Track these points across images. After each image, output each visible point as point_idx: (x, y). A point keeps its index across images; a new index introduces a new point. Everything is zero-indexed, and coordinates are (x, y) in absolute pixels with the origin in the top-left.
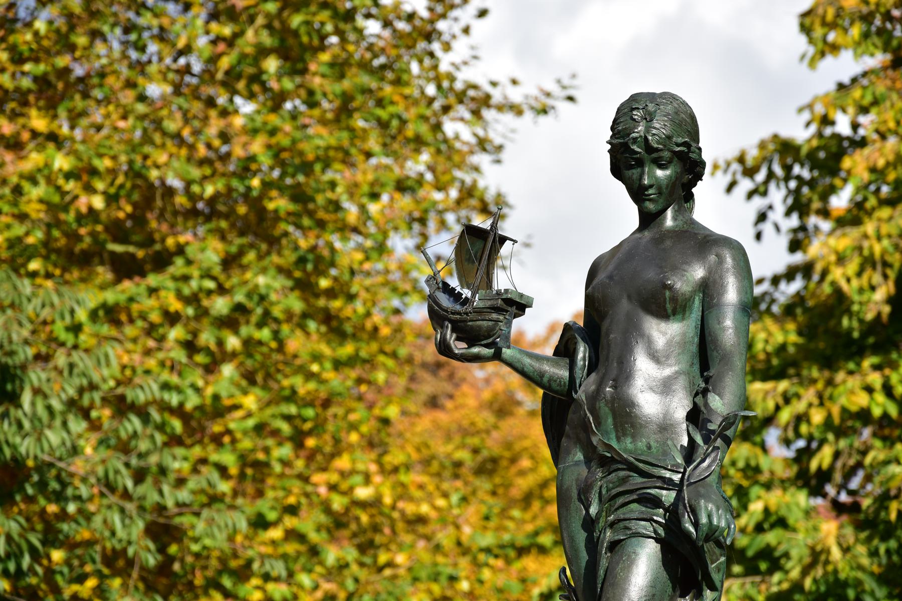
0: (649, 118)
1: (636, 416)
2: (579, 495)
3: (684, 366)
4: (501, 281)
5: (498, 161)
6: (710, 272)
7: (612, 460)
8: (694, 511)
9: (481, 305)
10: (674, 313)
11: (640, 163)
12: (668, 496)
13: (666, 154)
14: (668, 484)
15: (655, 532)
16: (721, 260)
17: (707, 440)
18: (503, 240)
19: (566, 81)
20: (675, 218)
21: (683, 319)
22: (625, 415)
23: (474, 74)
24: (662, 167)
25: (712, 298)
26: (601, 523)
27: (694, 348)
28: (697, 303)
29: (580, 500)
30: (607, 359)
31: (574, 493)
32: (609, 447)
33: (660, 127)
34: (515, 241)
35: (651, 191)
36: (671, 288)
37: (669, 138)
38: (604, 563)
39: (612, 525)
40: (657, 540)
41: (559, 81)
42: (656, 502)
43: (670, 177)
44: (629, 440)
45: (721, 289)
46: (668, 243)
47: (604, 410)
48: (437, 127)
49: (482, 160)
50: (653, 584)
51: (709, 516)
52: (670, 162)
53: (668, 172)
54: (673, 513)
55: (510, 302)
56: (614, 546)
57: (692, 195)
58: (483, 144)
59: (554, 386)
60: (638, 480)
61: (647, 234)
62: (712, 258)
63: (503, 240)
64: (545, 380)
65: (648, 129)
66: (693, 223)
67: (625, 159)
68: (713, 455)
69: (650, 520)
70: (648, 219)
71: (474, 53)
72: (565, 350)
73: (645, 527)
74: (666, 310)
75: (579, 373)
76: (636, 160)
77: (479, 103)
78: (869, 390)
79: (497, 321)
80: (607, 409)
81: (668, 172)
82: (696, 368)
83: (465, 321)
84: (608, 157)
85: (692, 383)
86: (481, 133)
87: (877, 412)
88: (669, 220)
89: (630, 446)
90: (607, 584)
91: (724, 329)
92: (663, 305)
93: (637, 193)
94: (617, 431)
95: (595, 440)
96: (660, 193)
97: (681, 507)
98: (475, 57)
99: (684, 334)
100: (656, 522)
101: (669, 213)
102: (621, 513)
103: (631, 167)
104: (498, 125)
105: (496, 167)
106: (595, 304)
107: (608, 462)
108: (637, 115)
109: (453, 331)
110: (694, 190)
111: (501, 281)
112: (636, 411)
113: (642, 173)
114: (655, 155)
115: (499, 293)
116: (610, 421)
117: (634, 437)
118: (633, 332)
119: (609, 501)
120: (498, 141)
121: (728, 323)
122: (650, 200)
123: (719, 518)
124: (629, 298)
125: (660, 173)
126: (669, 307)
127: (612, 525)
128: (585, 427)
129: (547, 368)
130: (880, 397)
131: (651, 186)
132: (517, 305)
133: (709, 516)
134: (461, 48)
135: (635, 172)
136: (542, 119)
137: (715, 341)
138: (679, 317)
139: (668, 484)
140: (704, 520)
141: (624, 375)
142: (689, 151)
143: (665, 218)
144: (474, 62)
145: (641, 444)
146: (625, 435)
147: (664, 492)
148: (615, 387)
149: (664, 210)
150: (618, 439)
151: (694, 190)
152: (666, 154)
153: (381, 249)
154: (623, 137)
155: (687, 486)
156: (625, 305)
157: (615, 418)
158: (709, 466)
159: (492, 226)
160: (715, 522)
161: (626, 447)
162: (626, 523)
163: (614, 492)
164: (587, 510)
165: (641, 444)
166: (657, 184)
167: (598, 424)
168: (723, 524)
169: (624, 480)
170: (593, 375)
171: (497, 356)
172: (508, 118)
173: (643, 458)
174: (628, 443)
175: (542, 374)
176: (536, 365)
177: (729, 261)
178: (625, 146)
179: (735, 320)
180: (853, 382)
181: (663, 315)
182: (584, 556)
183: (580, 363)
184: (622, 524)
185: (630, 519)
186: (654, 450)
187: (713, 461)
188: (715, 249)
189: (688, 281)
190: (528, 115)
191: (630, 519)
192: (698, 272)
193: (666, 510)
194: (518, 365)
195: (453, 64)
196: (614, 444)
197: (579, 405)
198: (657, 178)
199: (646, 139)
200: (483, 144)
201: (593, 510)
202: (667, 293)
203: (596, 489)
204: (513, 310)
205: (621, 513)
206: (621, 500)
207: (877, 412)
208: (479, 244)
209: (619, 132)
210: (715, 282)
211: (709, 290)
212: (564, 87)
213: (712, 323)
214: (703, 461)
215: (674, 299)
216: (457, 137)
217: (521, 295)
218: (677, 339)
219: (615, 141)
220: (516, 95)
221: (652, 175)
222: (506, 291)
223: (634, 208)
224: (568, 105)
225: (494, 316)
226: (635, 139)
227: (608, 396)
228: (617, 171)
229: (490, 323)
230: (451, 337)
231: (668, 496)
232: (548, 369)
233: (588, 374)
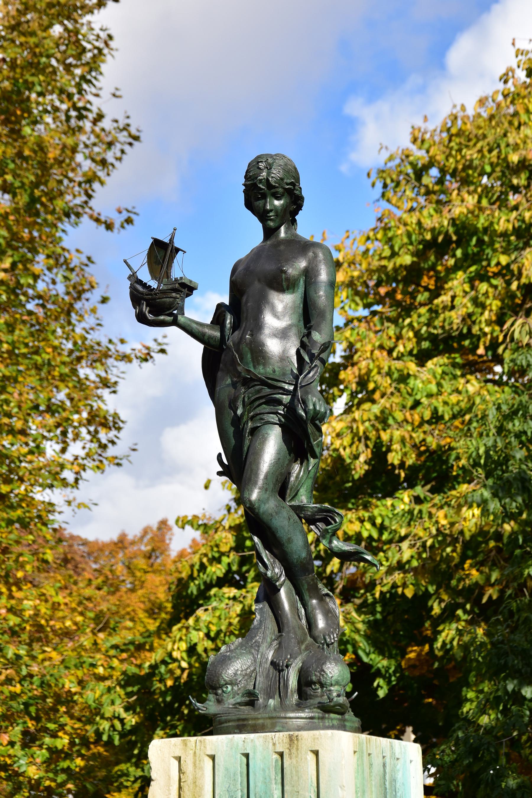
0: (269, 168)
1: (266, 352)
2: (230, 404)
3: (295, 321)
4: (176, 273)
5: (114, 392)
6: (309, 263)
7: (252, 380)
8: (304, 402)
9: (165, 288)
10: (288, 289)
11: (264, 197)
12: (286, 399)
13: (280, 190)
14: (286, 392)
15: (280, 420)
16: (316, 256)
17: (312, 359)
18: (177, 250)
19: (160, 340)
20: (286, 233)
21: (293, 292)
22: (259, 353)
23: (99, 336)
24: (278, 199)
25: (311, 279)
26: (245, 419)
27: (301, 311)
28: (302, 283)
29: (230, 407)
30: (246, 318)
31: (227, 403)
32: (249, 371)
33: (276, 173)
34: (185, 252)
35: (271, 214)
36: (285, 272)
37: (282, 179)
38: (247, 442)
39: (252, 418)
40: (280, 425)
41: (155, 340)
42: (279, 402)
43: (283, 205)
44: (261, 367)
45: (317, 274)
46: (282, 247)
47: (245, 349)
48: (74, 372)
49: (105, 393)
50: (278, 453)
51: (314, 405)
52: (283, 195)
53: (282, 202)
54: (291, 408)
55: (183, 285)
56: (254, 431)
57: (295, 220)
58: (105, 383)
59: (212, 341)
60: (267, 391)
61: (268, 243)
62: (311, 254)
63: (177, 250)
64: (206, 338)
65: (269, 174)
66: (297, 235)
67: (255, 194)
68: (315, 369)
69: (276, 413)
70: (269, 233)
71: (98, 322)
72: (218, 318)
73: (274, 418)
74: (282, 286)
75: (227, 332)
76: (261, 194)
77: (100, 356)
78: (362, 521)
79: (176, 298)
80: (247, 349)
81: (282, 202)
82: (302, 323)
83: (155, 299)
84: (242, 195)
85: (299, 332)
86: (103, 374)
87: (365, 534)
88: (282, 233)
89: (262, 371)
90: (250, 453)
91: (320, 297)
92: (280, 283)
93: (262, 216)
94: (253, 362)
95: (239, 369)
96: (277, 215)
97: (296, 401)
98: (99, 325)
99: (294, 302)
100: (280, 414)
101: (282, 229)
102: (258, 411)
103: (258, 199)
104: (116, 369)
105: (113, 395)
106: (237, 288)
107: (248, 381)
108: (262, 165)
109: (147, 306)
110: (296, 217)
111: (176, 273)
112: (266, 348)
113: (266, 202)
114: (273, 191)
115: (176, 280)
116: (249, 356)
117: (264, 365)
118: (261, 303)
119: (249, 405)
120: (113, 379)
121: (321, 293)
122: (271, 220)
123: (320, 406)
124: (259, 280)
125: (277, 203)
126: (284, 284)
127: (252, 418)
128: (234, 362)
129: (207, 331)
130: (368, 525)
131: (271, 211)
132: (188, 289)
133: (314, 405)
134: (90, 321)
135: (261, 203)
136: (144, 364)
137: (314, 304)
138: (291, 291)
139: (286, 392)
140: (311, 407)
141: (258, 326)
142: (294, 189)
143: (280, 232)
144: (99, 327)
145: (269, 370)
146: (259, 364)
147: (284, 397)
148: (252, 335)
149: (279, 228)
150: (255, 367)
151: (296, 217)
152: (280, 190)
153: (39, 450)
154: (253, 180)
155: (301, 387)
156: (257, 286)
157: (252, 354)
158: (313, 376)
159: (170, 240)
160: (318, 408)
161: (260, 371)
162: (261, 416)
163: (253, 398)
164: (235, 413)
165: (269, 370)
166: (275, 209)
167: (241, 359)
168: (323, 410)
169: (259, 391)
170: (236, 333)
171: (175, 323)
172: (122, 365)
173: (271, 376)
174: (261, 369)
175: (204, 334)
176: (200, 329)
177: (321, 255)
178: (255, 185)
179: (325, 292)
180: (351, 515)
181: (281, 290)
182: (233, 442)
183: (228, 326)
184: (258, 417)
185: (263, 413)
186: (277, 373)
187: (316, 373)
188: (312, 250)
189: (296, 269)
190: (135, 362)
191: (263, 413)
192: (303, 264)
193: (285, 406)
194: (188, 328)
195: (84, 329)
196: (252, 369)
197: (228, 348)
198: (275, 206)
199: (268, 180)
200: (105, 383)
201: (239, 412)
202: (284, 275)
203: (241, 399)
204: (186, 291)
205: (258, 411)
206: (257, 403)
207: (365, 534)
208: (162, 253)
209: (251, 177)
210: (313, 269)
211: (309, 275)
212: (160, 344)
213: (312, 293)
214: (309, 373)
215: (288, 279)
216: (87, 379)
217: (191, 281)
218: (290, 305)
219: (248, 183)
220: (126, 349)
221: (272, 204)
222: (181, 278)
223: (260, 225)
224: (161, 355)
225: (174, 295)
226: (261, 180)
227: (248, 341)
228: (249, 205)
229: (171, 300)
230: (146, 309)
231: (286, 399)
232: (208, 332)
233: (233, 333)
